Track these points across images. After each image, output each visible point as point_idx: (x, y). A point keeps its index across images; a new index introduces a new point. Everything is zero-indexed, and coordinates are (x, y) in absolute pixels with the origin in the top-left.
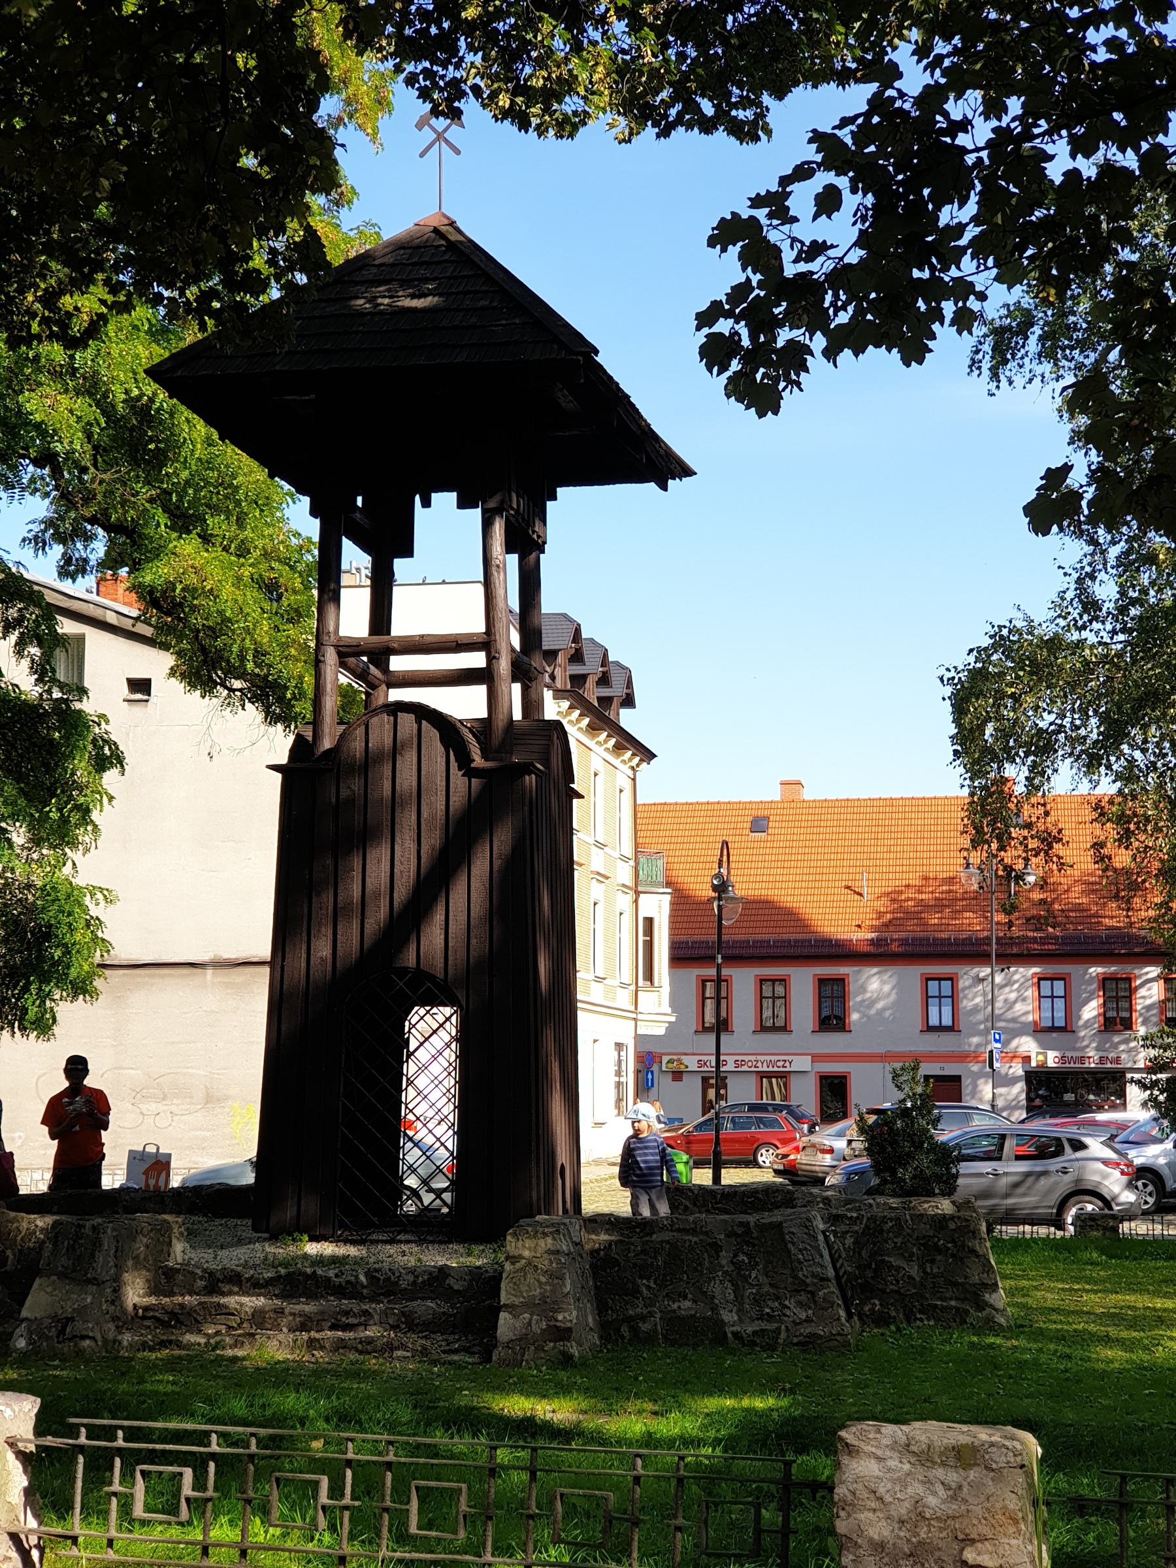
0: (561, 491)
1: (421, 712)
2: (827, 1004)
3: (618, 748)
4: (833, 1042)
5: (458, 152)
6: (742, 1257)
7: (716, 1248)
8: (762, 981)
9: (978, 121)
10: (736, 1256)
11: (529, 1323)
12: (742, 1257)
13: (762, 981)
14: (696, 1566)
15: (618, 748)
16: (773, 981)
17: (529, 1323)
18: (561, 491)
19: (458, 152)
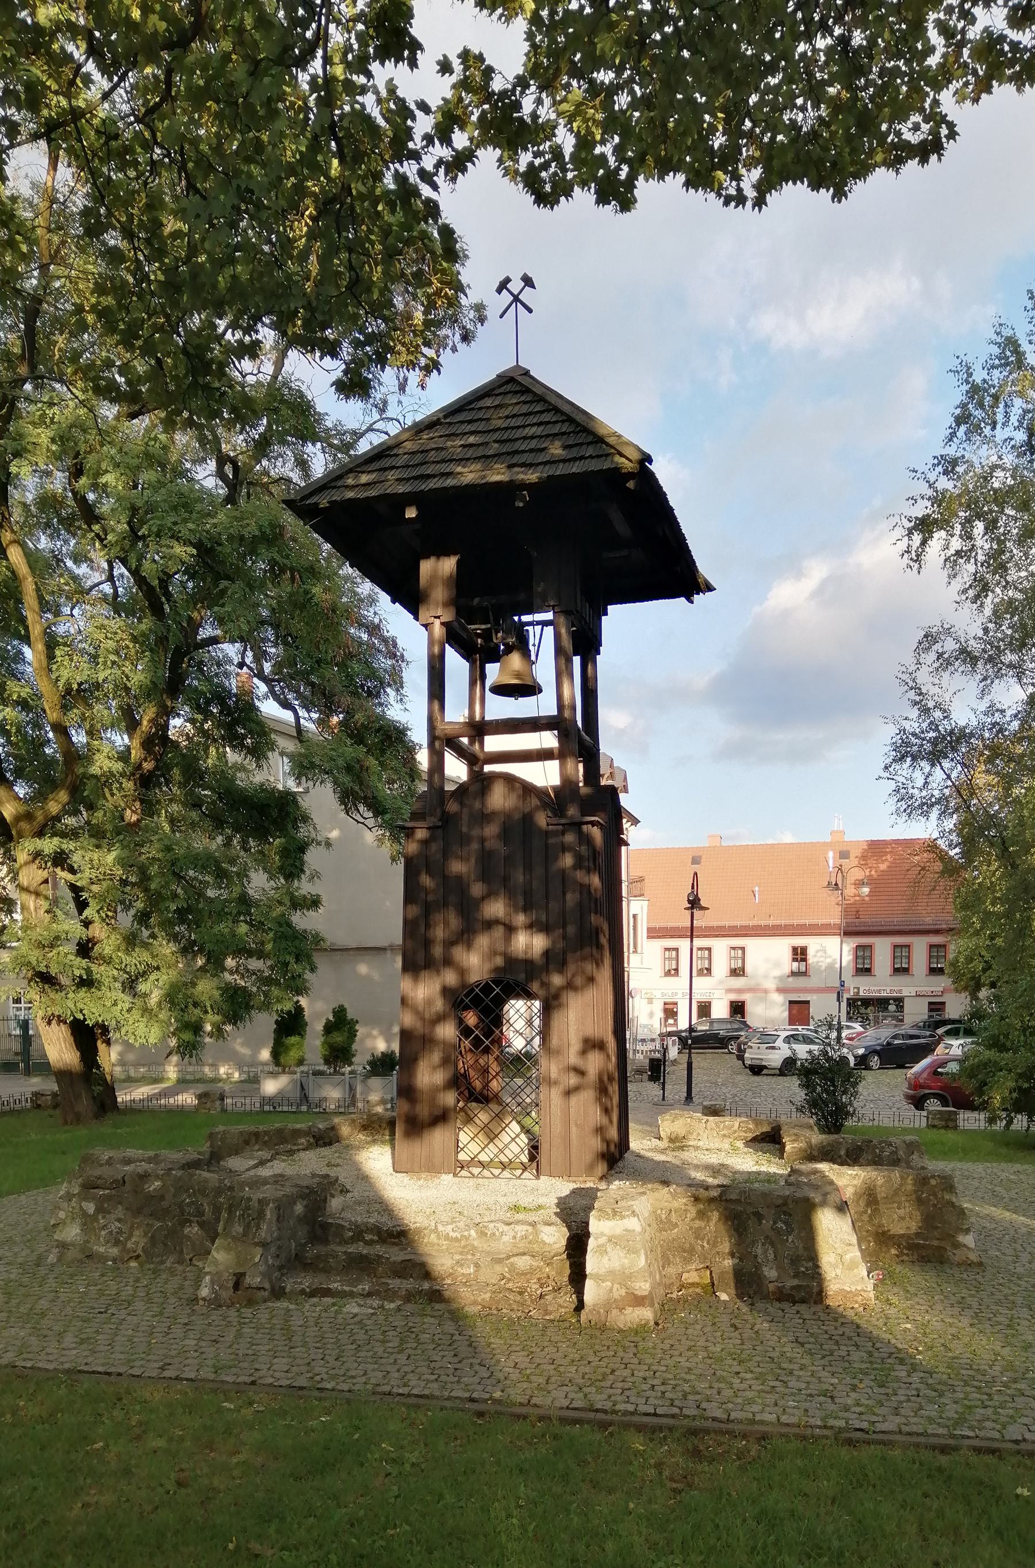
0: (611, 608)
1: (510, 780)
2: (860, 961)
3: (924, 161)
4: (738, 982)
5: (530, 311)
6: (780, 1225)
7: (759, 1216)
8: (931, 946)
9: (923, 125)
10: (775, 1223)
11: (611, 1290)
12: (780, 1225)
13: (931, 946)
14: (310, 6)
15: (924, 161)
16: (901, 946)
17: (611, 1290)
18: (611, 608)
19: (530, 311)
